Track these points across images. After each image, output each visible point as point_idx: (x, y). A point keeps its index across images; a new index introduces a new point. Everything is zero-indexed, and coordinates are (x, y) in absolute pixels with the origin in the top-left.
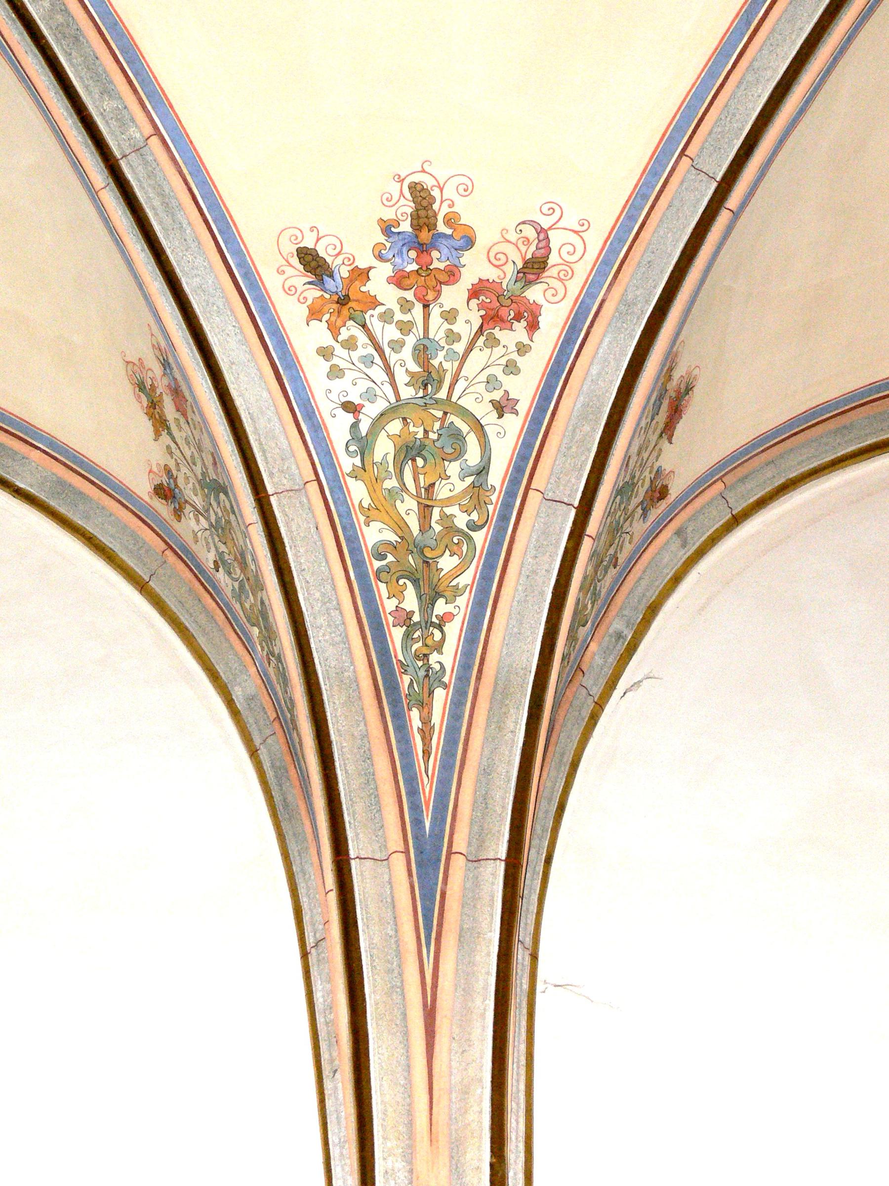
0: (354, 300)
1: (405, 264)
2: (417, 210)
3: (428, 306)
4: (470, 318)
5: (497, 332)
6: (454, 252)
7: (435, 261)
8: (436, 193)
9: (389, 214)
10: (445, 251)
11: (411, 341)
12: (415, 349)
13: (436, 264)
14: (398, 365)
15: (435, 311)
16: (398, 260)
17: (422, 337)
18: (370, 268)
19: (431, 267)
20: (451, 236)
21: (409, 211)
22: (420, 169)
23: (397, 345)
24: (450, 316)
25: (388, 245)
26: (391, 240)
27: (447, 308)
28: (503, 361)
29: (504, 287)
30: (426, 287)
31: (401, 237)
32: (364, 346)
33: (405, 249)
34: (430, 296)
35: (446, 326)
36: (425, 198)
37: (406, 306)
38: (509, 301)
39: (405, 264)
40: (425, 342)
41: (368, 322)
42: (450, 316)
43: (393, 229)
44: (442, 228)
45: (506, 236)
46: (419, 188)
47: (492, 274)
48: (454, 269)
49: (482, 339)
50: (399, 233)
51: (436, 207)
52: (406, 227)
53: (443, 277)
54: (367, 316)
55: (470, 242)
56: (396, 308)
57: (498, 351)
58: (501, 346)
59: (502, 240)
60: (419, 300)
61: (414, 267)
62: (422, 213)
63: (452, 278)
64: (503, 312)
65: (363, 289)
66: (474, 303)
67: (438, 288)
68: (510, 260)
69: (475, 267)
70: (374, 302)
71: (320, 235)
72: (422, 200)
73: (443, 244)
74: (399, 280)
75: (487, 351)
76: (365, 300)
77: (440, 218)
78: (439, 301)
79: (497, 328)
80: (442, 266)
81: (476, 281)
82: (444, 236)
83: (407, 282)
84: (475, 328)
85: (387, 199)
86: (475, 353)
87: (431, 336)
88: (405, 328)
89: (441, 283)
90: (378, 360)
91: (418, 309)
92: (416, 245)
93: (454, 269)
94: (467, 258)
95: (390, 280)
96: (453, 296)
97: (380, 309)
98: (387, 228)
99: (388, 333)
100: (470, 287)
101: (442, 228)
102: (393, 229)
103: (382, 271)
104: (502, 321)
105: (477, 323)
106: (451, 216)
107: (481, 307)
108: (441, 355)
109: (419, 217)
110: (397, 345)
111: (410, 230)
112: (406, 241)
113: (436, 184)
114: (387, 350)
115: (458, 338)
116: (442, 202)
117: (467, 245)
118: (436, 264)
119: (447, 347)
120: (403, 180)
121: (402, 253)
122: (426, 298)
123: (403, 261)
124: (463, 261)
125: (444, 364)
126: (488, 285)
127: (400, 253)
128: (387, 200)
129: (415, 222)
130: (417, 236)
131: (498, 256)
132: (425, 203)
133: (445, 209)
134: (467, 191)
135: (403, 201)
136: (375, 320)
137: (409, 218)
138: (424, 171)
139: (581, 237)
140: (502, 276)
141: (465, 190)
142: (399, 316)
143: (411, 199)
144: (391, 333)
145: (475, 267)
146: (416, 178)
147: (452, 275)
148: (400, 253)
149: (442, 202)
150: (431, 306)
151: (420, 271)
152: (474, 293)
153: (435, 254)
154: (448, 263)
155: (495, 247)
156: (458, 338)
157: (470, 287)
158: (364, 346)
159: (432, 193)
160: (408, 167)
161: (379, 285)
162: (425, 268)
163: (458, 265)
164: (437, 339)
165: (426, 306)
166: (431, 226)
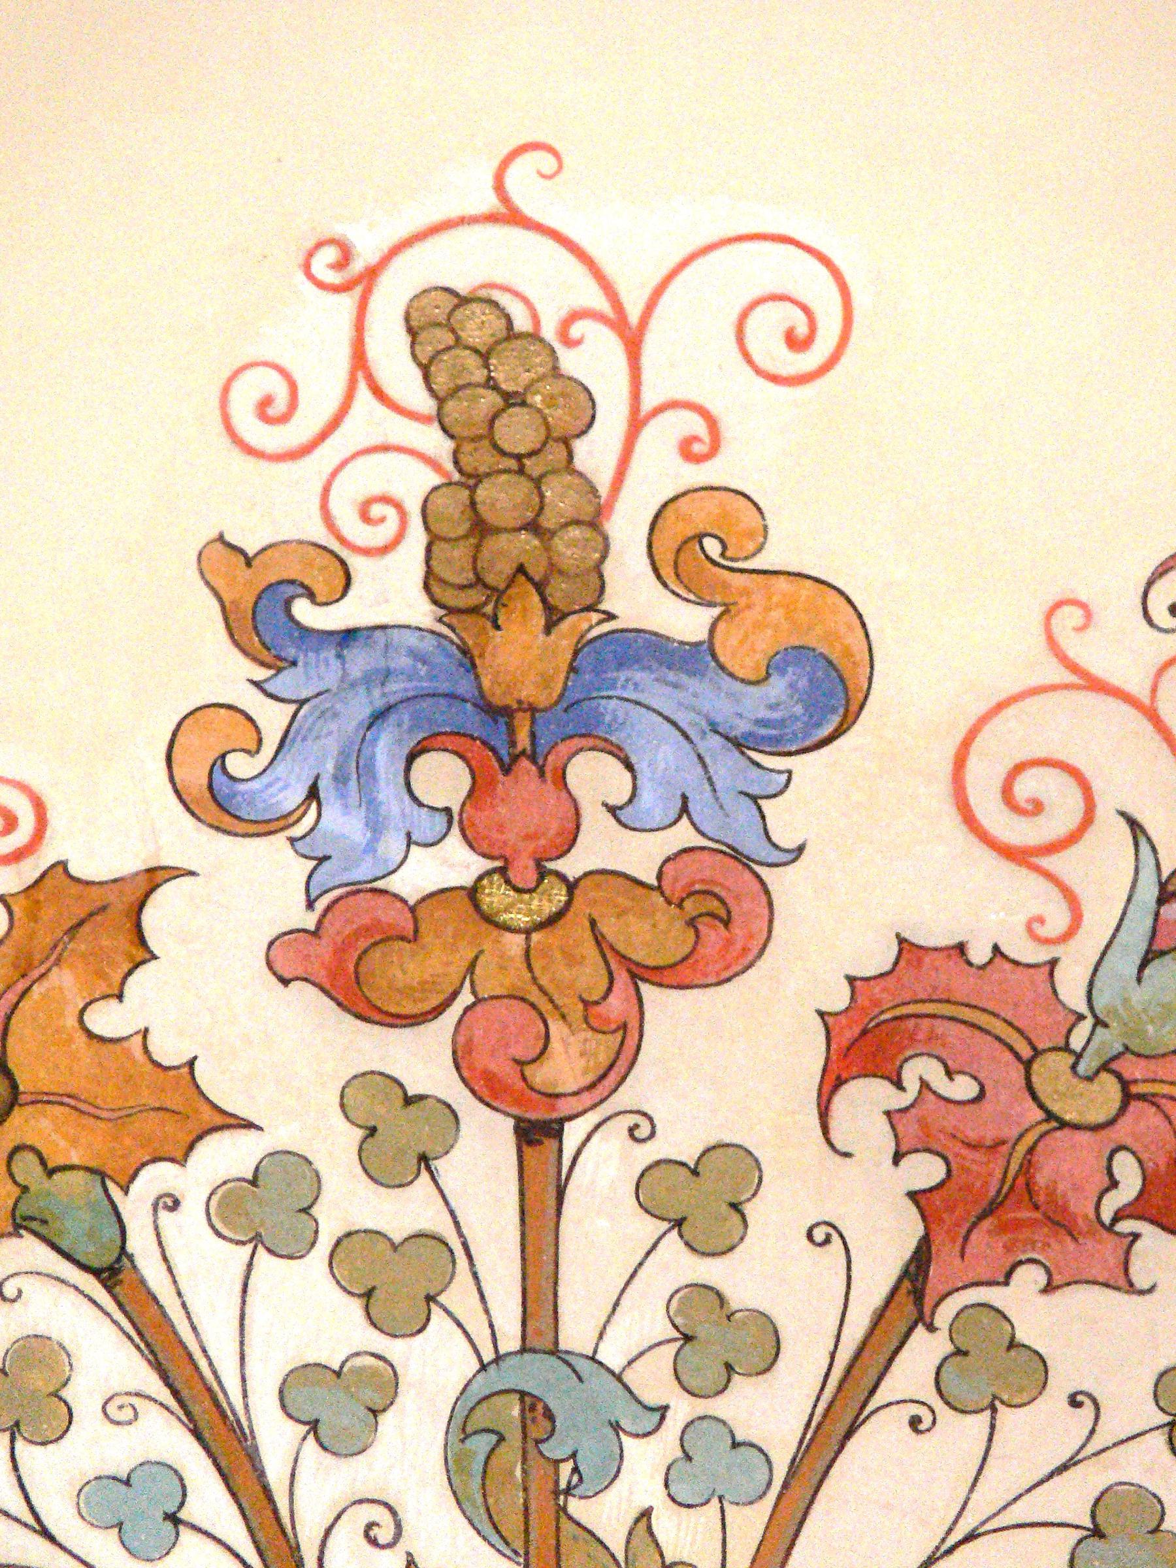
0: (43, 1099)
1: (393, 845)
2: (472, 480)
3: (554, 1130)
4: (834, 1216)
5: (1024, 1303)
6: (727, 766)
7: (595, 822)
8: (595, 361)
9: (274, 511)
10: (662, 755)
11: (436, 1366)
12: (463, 1424)
13: (599, 848)
14: (347, 1536)
15: (602, 1165)
16: (340, 821)
17: (510, 1341)
18: (155, 877)
19: (572, 865)
20: (696, 658)
21: (413, 482)
22: (489, 202)
23: (343, 1403)
24: (702, 1197)
25: (273, 718)
26: (288, 683)
27: (680, 1141)
28: (1072, 1499)
29: (1072, 993)
30: (536, 1003)
31: (360, 660)
32: (118, 1410)
33: (386, 751)
34: (566, 1065)
35: (677, 1265)
36: (513, 400)
37: (397, 1135)
38: (1110, 1087)
39: (393, 845)
40: (536, 1375)
41: (140, 1243)
42: (702, 1197)
43: (302, 610)
44: (638, 598)
45: (1079, 649)
46: (478, 328)
47: (987, 909)
48: (735, 879)
49: (922, 1354)
50: (348, 636)
51: (596, 454)
52: (392, 593)
53: (649, 935)
54: (135, 1205)
55: (830, 693)
56: (334, 1147)
57: (1037, 1432)
58: (1054, 1399)
59: (1062, 675)
60: (488, 1090)
61: (451, 864)
62: (502, 497)
63: (713, 935)
64: (1066, 1166)
65: (107, 1020)
66: (866, 1103)
67: (617, 1006)
68: (1105, 812)
69: (868, 863)
70: (184, 1112)
71: (293, 707)
72: (499, 398)
73: (644, 708)
74: (350, 956)
75: (962, 1433)
76: (109, 1095)
77: (627, 528)
78: (624, 1097)
79: (1029, 1278)
80: (641, 856)
81: (877, 957)
82: (652, 649)
83: (401, 971)
84: (877, 1276)
85: (265, 403)
86: (879, 1442)
87: (576, 1333)
88: (396, 1282)
89: (639, 973)
90: (210, 1501)
91: (482, 1158)
92: (470, 719)
93: (735, 879)
94: (815, 796)
95: (285, 960)
96: (724, 1061)
97: (224, 1157)
98: (265, 605)
99: (282, 1322)
100: (839, 999)
101: (638, 598)
102: (302, 610)
103: (235, 903)
104: (1061, 1222)
105: (886, 1240)
106: (700, 514)
107: (908, 1135)
108: (645, 1461)
109: (481, 528)
110: (343, 1403)
111: (422, 613)
112: (396, 688)
113: (601, 303)
114: (275, 1438)
115: (764, 1346)
116: (636, 424)
117: (816, 710)
118: (599, 848)
119: (682, 1409)
120: (372, 274)
121: (366, 772)
122: (540, 1075)
123: (376, 827)
124: (786, 820)
125: (666, 1524)
126: (963, 985)
127: (355, 768)
128: (261, 419)
129: (455, 563)
130: (468, 659)
131: (1025, 787)
132: (517, 431)
133: (658, 473)
134: (810, 348)
135: (368, 420)
136: (188, 1231)
137: (417, 539)
138: (509, 215)
139: (759, 809)
140: (1058, 921)
141: (796, 343)
142: (350, 1201)
143: (424, 403)
144: (302, 1316)
145: (868, 863)
146: (461, 262)
147: (714, 915)
148: (355, 768)
149: (636, 424)
150: (574, 1133)
151: (496, 896)
152: (864, 1040)
153: (594, 777)
154: (684, 835)
155: (975, 767)
156: (764, 1346)
157: (839, 999)
158: (118, 1410)
159: (569, 361)
160: (409, 190)
161: (214, 989)
162: (524, 872)
163: (752, 845)
164: (612, 1355)
165: (537, 1133)
166: (564, 590)
